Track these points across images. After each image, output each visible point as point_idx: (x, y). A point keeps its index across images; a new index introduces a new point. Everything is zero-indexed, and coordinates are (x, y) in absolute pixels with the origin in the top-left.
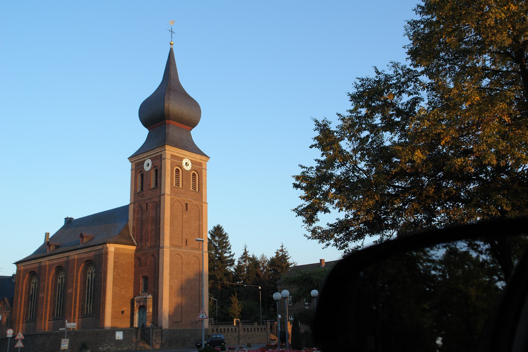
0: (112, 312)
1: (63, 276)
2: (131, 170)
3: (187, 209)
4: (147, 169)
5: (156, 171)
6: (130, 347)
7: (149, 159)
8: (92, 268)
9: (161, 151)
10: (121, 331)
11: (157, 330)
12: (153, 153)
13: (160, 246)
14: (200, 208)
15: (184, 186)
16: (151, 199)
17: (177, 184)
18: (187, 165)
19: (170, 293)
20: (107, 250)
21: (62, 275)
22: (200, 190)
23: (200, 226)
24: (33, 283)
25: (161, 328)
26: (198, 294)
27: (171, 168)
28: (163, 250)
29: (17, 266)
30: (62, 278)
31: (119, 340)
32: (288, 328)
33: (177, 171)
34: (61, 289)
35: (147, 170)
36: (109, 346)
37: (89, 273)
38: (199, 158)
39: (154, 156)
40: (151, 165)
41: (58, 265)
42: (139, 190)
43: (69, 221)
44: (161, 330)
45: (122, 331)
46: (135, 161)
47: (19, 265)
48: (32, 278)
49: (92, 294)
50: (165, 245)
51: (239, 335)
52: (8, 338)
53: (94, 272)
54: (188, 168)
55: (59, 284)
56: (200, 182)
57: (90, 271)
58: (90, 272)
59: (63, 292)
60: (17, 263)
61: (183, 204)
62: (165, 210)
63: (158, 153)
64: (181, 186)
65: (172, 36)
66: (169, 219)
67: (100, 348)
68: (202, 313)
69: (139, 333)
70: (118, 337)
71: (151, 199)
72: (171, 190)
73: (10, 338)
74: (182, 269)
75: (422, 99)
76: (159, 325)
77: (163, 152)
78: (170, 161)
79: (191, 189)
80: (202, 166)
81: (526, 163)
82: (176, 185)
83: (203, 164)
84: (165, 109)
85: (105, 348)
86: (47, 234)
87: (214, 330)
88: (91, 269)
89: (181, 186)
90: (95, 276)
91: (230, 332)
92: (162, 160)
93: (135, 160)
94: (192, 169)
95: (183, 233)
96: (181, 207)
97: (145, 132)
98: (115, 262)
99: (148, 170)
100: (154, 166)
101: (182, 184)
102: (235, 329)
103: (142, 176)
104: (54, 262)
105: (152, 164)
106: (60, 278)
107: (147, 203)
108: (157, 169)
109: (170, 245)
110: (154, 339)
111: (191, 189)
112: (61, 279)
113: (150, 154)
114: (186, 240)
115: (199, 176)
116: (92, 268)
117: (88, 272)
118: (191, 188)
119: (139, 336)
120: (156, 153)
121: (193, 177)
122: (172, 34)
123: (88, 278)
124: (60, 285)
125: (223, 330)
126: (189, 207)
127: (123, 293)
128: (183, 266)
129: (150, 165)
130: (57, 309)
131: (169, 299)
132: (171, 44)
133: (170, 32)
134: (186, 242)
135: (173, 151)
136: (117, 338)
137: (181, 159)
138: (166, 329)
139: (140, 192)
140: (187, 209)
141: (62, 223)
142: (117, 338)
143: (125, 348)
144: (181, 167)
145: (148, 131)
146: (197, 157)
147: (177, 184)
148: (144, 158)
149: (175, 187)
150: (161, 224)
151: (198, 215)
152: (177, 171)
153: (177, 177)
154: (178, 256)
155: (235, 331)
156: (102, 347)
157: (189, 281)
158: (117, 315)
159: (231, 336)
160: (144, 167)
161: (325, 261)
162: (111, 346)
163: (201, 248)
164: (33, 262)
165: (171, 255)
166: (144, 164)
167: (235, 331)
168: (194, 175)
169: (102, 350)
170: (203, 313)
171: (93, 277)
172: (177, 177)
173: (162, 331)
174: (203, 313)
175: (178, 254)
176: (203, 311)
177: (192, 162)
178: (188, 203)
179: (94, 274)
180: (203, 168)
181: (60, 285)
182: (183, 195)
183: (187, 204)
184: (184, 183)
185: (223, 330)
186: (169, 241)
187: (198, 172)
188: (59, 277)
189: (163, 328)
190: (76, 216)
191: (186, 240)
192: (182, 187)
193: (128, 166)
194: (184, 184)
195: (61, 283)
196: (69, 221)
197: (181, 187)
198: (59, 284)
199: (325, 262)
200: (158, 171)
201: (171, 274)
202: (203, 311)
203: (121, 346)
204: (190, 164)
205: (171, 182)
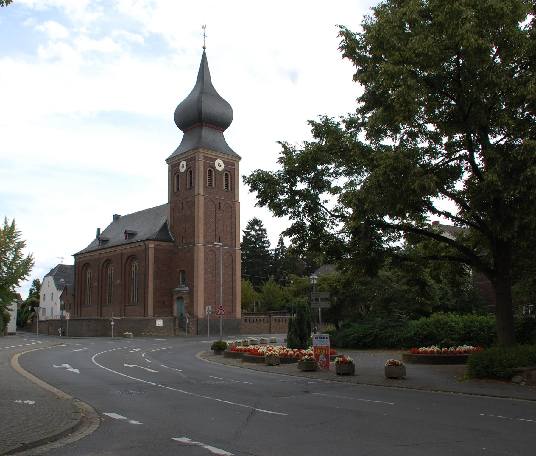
0: (154, 301)
3: (220, 208)
4: (182, 170)
5: (191, 172)
6: (169, 333)
7: (184, 161)
8: (136, 262)
9: (195, 153)
11: (193, 319)
12: (187, 155)
14: (233, 207)
16: (187, 198)
17: (211, 184)
18: (220, 165)
19: (204, 286)
21: (136, 263)
22: (233, 189)
24: (88, 273)
25: (197, 317)
26: (232, 287)
27: (204, 169)
28: (198, 247)
29: (75, 258)
30: (112, 270)
31: (159, 327)
33: (210, 172)
34: (111, 280)
35: (182, 172)
36: (151, 332)
37: (133, 267)
38: (231, 158)
39: (188, 158)
40: (186, 167)
41: (107, 259)
42: (175, 190)
43: (116, 217)
44: (196, 319)
47: (77, 257)
48: (88, 269)
49: (137, 286)
51: (270, 325)
52: (66, 320)
53: (138, 266)
54: (220, 169)
55: (109, 275)
56: (233, 181)
57: (135, 265)
58: (134, 266)
59: (113, 282)
60: (75, 256)
61: (216, 203)
63: (192, 155)
64: (214, 186)
66: (203, 218)
68: (220, 310)
69: (177, 322)
70: (159, 325)
71: (187, 198)
72: (204, 190)
73: (68, 320)
74: (216, 264)
75: (487, 22)
76: (195, 314)
77: (196, 154)
78: (203, 162)
79: (224, 189)
80: (234, 166)
82: (209, 185)
83: (235, 164)
84: (203, 116)
86: (99, 230)
87: (247, 320)
88: (135, 262)
89: (214, 186)
90: (138, 269)
91: (262, 322)
94: (224, 170)
95: (217, 231)
96: (214, 206)
97: (181, 134)
99: (184, 171)
100: (188, 169)
101: (215, 184)
102: (267, 319)
103: (178, 176)
104: (104, 255)
106: (109, 270)
108: (191, 171)
109: (204, 242)
110: (191, 327)
111: (224, 189)
112: (110, 271)
113: (185, 156)
114: (220, 237)
115: (231, 176)
116: (136, 262)
117: (133, 265)
118: (224, 187)
119: (177, 325)
120: (190, 155)
121: (226, 178)
123: (132, 270)
125: (255, 320)
126: (222, 206)
127: (163, 285)
128: (217, 262)
129: (185, 167)
130: (109, 297)
131: (204, 292)
133: (203, 37)
134: (220, 238)
135: (206, 152)
136: (157, 325)
137: (214, 160)
138: (201, 319)
139: (176, 192)
140: (220, 208)
141: (111, 220)
142: (157, 325)
144: (214, 168)
145: (183, 134)
146: (229, 158)
147: (211, 184)
148: (179, 159)
149: (208, 188)
152: (210, 172)
153: (210, 177)
155: (267, 321)
156: (144, 332)
159: (262, 325)
163: (234, 244)
164: (87, 255)
165: (205, 252)
166: (179, 166)
167: (267, 321)
168: (226, 175)
170: (221, 310)
171: (137, 270)
172: (210, 177)
173: (198, 320)
174: (221, 310)
175: (212, 251)
176: (221, 308)
177: (225, 162)
178: (221, 202)
179: (137, 268)
181: (110, 276)
184: (217, 183)
185: (255, 320)
186: (203, 238)
187: (231, 172)
188: (109, 269)
189: (199, 318)
190: (122, 214)
191: (220, 237)
192: (215, 187)
193: (166, 167)
195: (110, 274)
196: (116, 217)
197: (214, 187)
200: (191, 171)
201: (205, 268)
202: (221, 308)
203: (161, 332)
204: (223, 165)
205: (204, 182)
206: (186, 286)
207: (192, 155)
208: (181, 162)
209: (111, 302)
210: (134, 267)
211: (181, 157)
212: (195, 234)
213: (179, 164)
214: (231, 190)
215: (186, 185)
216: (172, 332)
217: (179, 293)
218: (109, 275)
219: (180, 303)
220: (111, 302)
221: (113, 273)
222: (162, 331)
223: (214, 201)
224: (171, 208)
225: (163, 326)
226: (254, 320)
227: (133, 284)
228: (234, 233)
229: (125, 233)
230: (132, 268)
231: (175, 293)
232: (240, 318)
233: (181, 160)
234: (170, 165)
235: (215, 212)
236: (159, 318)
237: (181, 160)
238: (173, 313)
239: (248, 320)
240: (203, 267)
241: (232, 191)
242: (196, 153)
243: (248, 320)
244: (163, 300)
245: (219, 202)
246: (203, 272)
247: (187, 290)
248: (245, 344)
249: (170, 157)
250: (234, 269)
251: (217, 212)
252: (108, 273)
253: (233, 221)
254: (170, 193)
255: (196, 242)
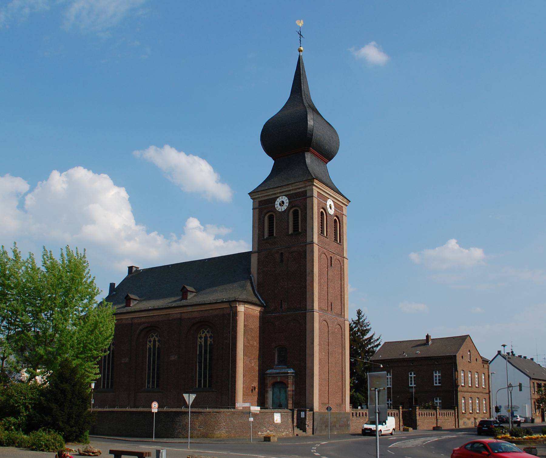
1: (157, 339)
2: (253, 209)
3: (331, 265)
5: (296, 213)
6: (288, 432)
9: (305, 187)
10: (279, 412)
12: (291, 188)
13: (307, 309)
15: (328, 235)
20: (236, 309)
22: (341, 241)
23: (342, 286)
30: (155, 341)
31: (277, 424)
32: (417, 413)
36: (268, 431)
39: (292, 192)
45: (280, 412)
46: (259, 197)
50: (314, 309)
56: (341, 230)
61: (328, 257)
62: (314, 263)
63: (299, 188)
65: (300, 40)
66: (317, 275)
67: (260, 433)
77: (308, 188)
81: (1, 291)
85: (264, 433)
86: (112, 285)
87: (354, 414)
92: (306, 198)
93: (260, 196)
97: (270, 162)
98: (245, 326)
103: (271, 218)
105: (290, 203)
107: (282, 253)
113: (286, 189)
114: (331, 303)
120: (296, 189)
122: (301, 38)
124: (152, 350)
125: (361, 415)
132: (300, 51)
139: (267, 239)
140: (331, 265)
143: (283, 434)
145: (273, 161)
148: (275, 194)
150: (308, 282)
151: (340, 273)
154: (325, 322)
157: (19, 354)
158: (248, 392)
160: (276, 206)
161: (432, 338)
162: (270, 431)
163: (343, 314)
168: (335, 220)
169: (261, 435)
173: (313, 413)
178: (332, 256)
179: (157, 344)
180: (343, 214)
182: (328, 245)
183: (331, 257)
184: (328, 230)
185: (361, 415)
187: (340, 219)
191: (331, 303)
194: (328, 231)
195: (152, 347)
198: (150, 349)
199: (431, 339)
206: (289, 368)
207: (299, 188)
208: (278, 197)
209: (108, 386)
210: (203, 339)
211: (279, 191)
212: (307, 296)
213: (275, 200)
214: (340, 242)
215: (288, 229)
216: (290, 430)
217: (277, 377)
218: (201, 346)
219: (276, 390)
220: (108, 386)
221: (157, 346)
222: (280, 430)
223: (326, 254)
224: (258, 259)
225: (281, 423)
226: (361, 413)
227: (200, 363)
228: (343, 299)
229: (181, 291)
230: (199, 340)
231: (269, 376)
232: (349, 411)
233: (278, 195)
234: (257, 201)
235: (328, 269)
236: (276, 410)
237: (278, 195)
238: (264, 403)
239: (354, 414)
240: (318, 343)
241: (341, 244)
242: (307, 186)
243: (354, 414)
244: (253, 385)
245: (331, 255)
246: (318, 348)
247: (293, 373)
248: (393, 446)
249: (252, 192)
250: (343, 347)
251: (329, 269)
252: (148, 346)
253: (342, 283)
254: (256, 239)
255: (308, 308)
